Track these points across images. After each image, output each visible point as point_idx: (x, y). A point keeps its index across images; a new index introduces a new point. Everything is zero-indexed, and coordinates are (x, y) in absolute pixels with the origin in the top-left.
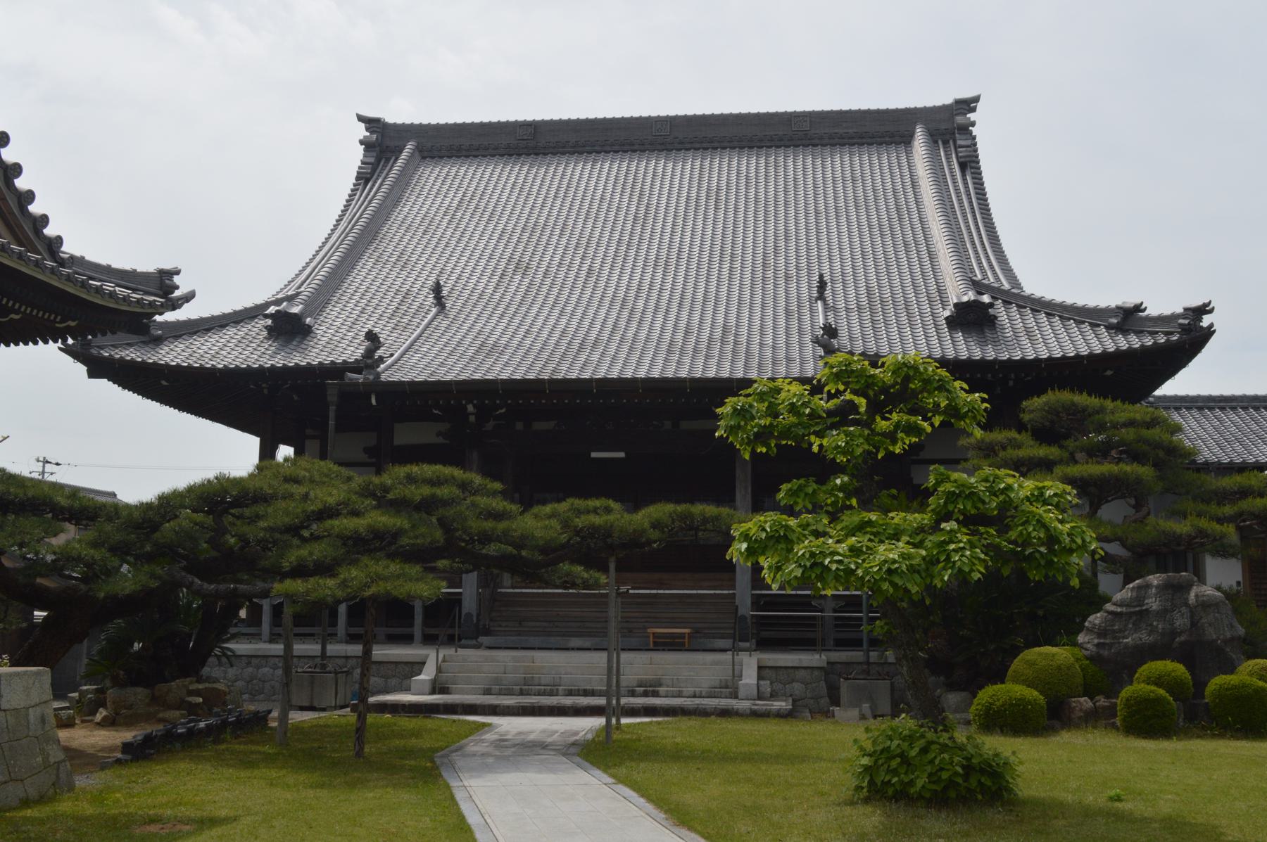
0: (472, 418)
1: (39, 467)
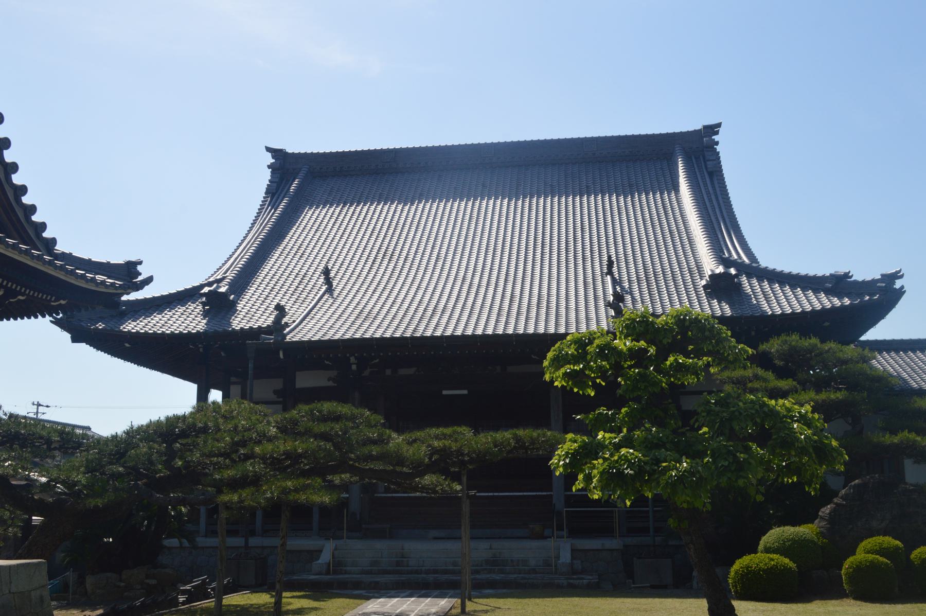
0: (354, 367)
1: (34, 409)
